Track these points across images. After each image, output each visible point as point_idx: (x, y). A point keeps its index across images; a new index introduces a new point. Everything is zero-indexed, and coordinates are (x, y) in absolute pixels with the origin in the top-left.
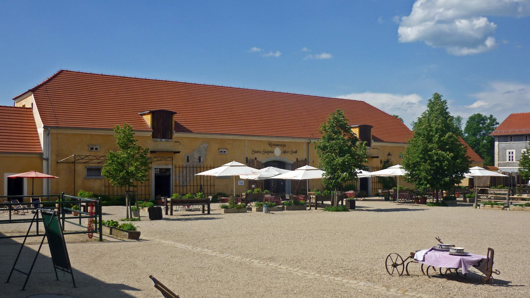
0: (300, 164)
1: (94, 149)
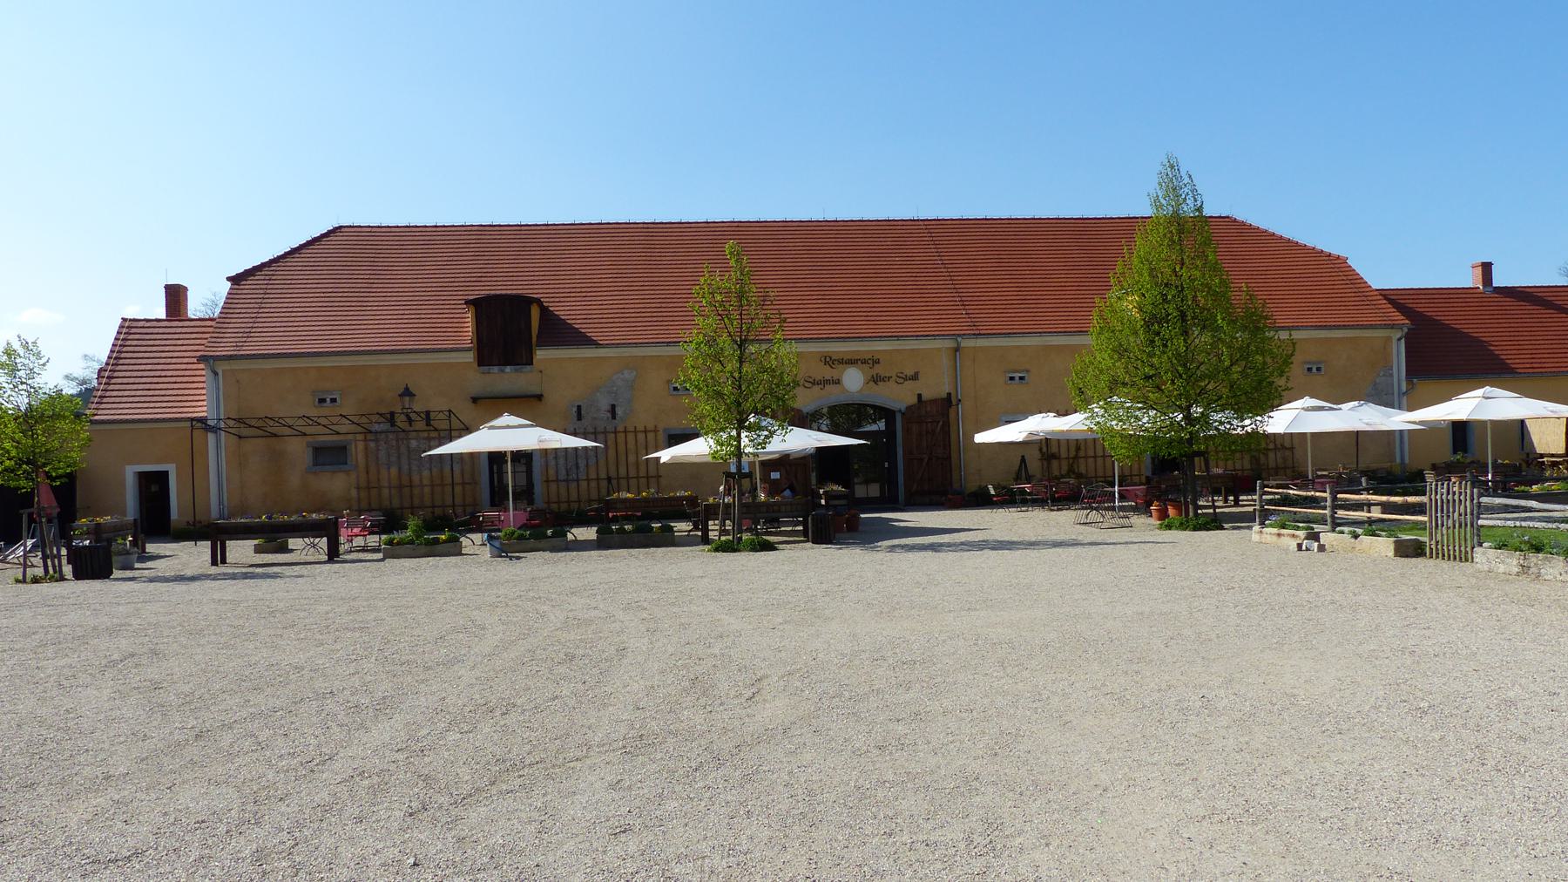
0: (929, 409)
1: (328, 400)
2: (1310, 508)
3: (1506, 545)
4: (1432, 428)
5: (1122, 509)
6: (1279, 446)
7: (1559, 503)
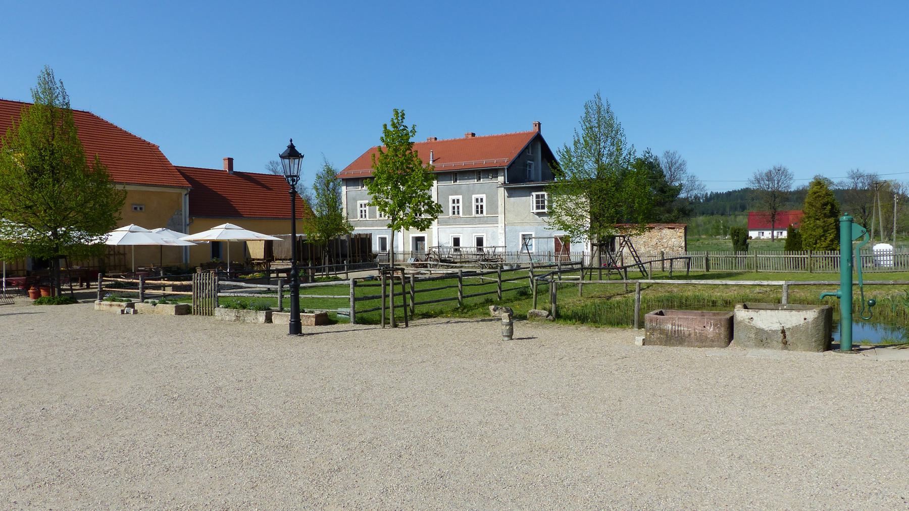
2: (129, 289)
3: (229, 306)
4: (201, 245)
5: (7, 292)
6: (117, 253)
7: (254, 284)
